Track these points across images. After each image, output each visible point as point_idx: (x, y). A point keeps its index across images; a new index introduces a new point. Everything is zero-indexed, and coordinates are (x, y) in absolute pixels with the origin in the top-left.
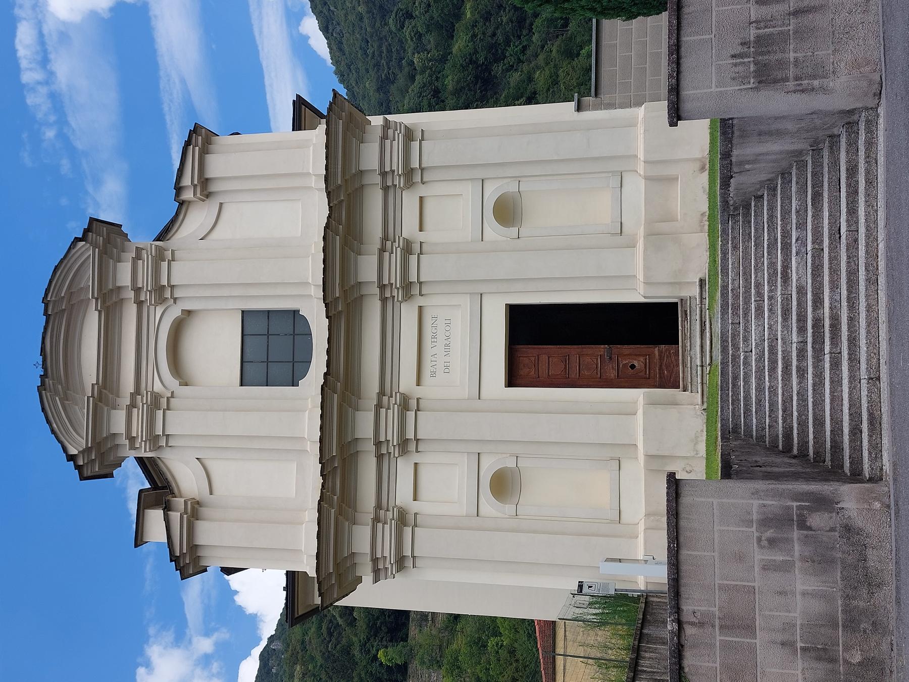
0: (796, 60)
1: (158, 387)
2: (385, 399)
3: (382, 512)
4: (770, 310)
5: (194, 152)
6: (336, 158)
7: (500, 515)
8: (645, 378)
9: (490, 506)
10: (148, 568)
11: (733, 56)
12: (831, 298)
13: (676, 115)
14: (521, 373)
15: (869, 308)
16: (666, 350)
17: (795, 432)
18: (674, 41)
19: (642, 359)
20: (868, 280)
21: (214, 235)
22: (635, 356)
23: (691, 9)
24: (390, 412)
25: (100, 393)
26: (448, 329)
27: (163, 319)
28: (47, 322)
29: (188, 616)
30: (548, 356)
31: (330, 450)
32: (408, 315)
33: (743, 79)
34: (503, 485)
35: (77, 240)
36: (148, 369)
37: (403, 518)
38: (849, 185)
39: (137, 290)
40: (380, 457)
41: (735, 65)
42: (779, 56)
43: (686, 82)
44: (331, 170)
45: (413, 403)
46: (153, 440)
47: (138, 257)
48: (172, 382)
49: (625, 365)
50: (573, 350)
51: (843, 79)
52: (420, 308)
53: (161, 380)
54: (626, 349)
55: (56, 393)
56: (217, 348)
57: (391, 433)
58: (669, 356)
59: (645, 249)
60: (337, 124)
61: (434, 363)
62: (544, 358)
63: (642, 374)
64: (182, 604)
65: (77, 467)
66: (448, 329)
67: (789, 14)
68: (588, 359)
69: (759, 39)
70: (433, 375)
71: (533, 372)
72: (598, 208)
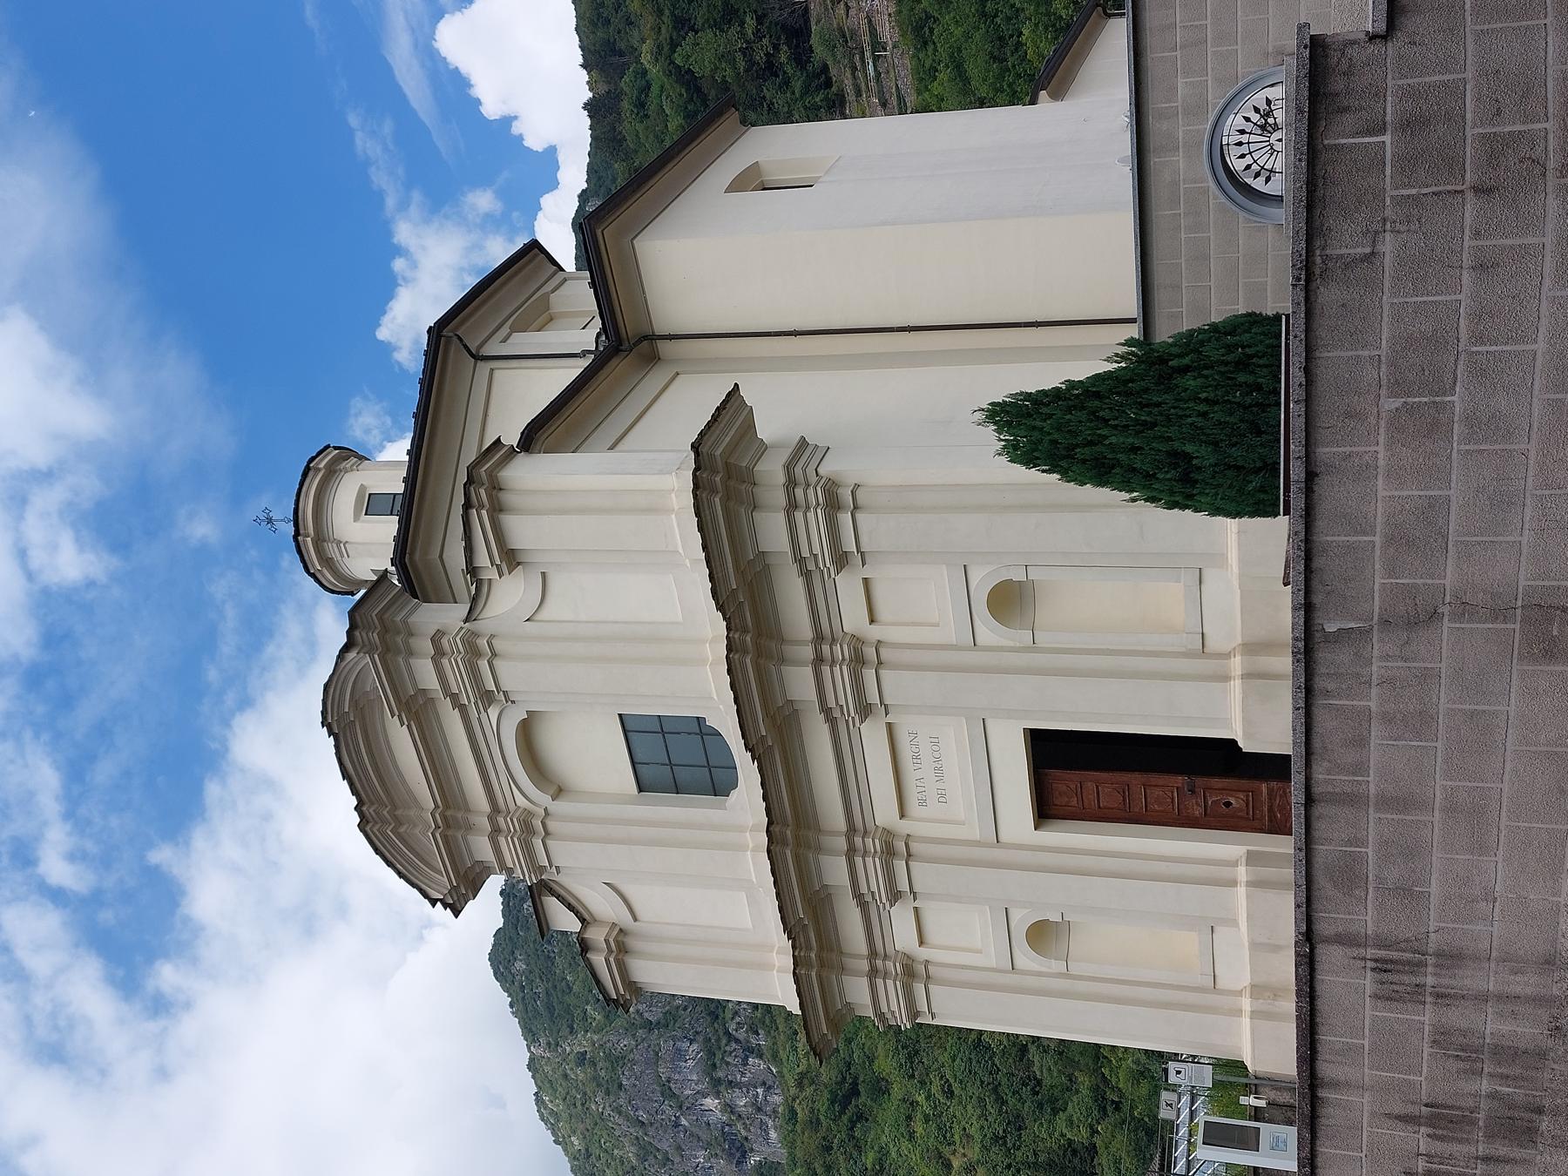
2: (799, 492)
7: (1044, 969)
9: (990, 631)
18: (1304, 928)
21: (543, 615)
23: (1332, 1121)
24: (811, 515)
25: (444, 818)
27: (504, 725)
28: (336, 740)
30: (1102, 785)
31: (757, 729)
32: (872, 736)
35: (346, 649)
36: (501, 783)
37: (910, 971)
40: (807, 575)
45: (870, 652)
47: (439, 653)
48: (543, 799)
50: (1135, 779)
53: (525, 794)
54: (1217, 782)
55: (384, 822)
56: (594, 756)
57: (873, 881)
60: (711, 506)
62: (1090, 786)
64: (389, 69)
65: (446, 906)
68: (1157, 792)
70: (923, 802)
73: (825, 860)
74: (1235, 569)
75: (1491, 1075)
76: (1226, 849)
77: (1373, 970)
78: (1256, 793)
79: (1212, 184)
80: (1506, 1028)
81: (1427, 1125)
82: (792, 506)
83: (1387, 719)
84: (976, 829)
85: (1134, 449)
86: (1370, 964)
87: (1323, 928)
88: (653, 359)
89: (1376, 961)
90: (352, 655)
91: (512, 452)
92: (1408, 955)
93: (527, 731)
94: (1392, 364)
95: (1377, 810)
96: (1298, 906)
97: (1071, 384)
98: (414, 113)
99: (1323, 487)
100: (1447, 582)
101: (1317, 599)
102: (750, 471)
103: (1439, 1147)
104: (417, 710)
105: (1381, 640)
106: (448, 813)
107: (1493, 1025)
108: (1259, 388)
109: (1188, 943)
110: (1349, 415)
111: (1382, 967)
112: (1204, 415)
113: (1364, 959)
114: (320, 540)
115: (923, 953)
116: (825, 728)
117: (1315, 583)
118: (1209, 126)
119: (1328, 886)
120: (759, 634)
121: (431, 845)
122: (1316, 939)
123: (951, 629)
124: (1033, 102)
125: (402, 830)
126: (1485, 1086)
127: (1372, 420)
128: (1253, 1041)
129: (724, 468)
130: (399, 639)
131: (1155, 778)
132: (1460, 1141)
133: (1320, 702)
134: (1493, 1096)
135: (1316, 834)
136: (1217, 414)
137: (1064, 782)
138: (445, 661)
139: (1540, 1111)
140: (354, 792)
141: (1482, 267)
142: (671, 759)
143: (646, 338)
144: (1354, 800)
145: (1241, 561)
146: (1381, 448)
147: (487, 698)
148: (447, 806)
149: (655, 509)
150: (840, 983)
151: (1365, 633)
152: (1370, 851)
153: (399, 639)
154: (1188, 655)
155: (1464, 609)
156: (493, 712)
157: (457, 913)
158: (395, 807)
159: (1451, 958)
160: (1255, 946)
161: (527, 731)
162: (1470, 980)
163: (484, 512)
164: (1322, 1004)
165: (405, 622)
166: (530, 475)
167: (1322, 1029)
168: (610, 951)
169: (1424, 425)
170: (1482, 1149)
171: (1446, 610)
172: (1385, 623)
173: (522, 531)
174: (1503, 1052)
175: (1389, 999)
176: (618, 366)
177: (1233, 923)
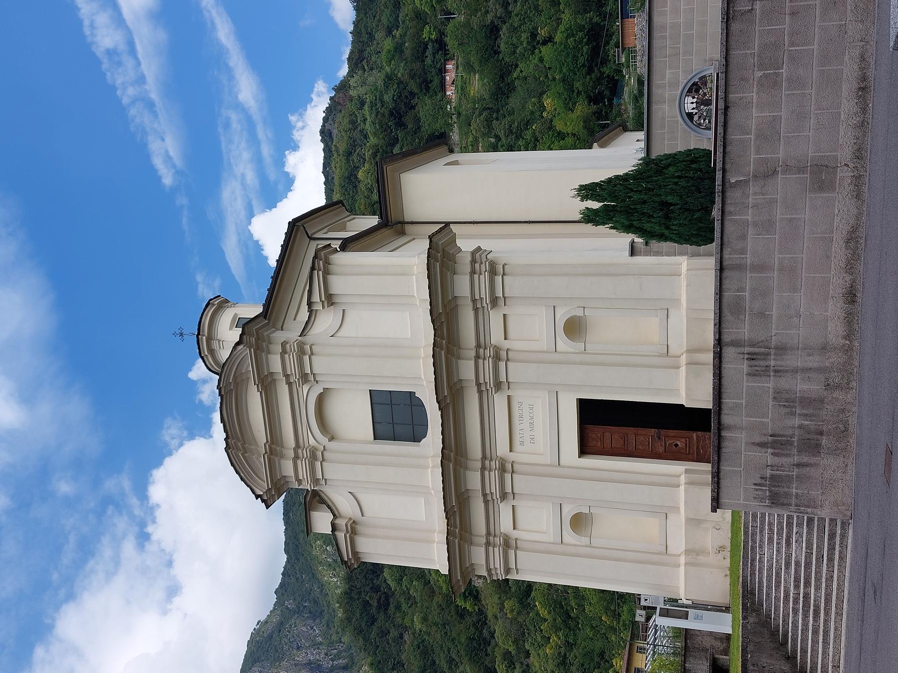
0: (797, 495)
1: (312, 442)
2: (477, 265)
3: (491, 538)
4: (777, 551)
5: (318, 276)
6: (437, 293)
7: (578, 543)
10: (185, 221)
11: (755, 484)
12: (815, 595)
13: (716, 504)
15: (836, 629)
17: (790, 634)
20: (837, 613)
21: (340, 334)
24: (482, 277)
27: (309, 394)
29: (230, 264)
30: (612, 434)
33: (762, 500)
34: (579, 522)
35: (238, 344)
37: (507, 544)
38: (829, 544)
39: (287, 376)
41: (757, 490)
42: (786, 490)
43: (722, 495)
44: (434, 304)
45: (503, 354)
46: (316, 481)
47: (284, 352)
48: (324, 440)
50: (630, 430)
51: (827, 511)
52: (509, 396)
53: (314, 438)
54: (672, 433)
55: (238, 449)
56: (354, 416)
58: (704, 440)
60: (435, 268)
62: (608, 435)
64: (222, 253)
65: (263, 501)
67: (794, 465)
68: (641, 438)
69: (772, 477)
70: (522, 443)
72: (650, 327)
73: (469, 473)
74: (685, 306)
75: (799, 415)
76: (676, 469)
77: (747, 359)
78: (691, 438)
79: (680, 119)
80: (805, 387)
81: (772, 448)
82: (473, 272)
83: (755, 224)
84: (548, 458)
85: (644, 202)
86: (746, 356)
87: (726, 338)
88: (402, 233)
89: (748, 354)
90: (241, 347)
91: (336, 251)
92: (762, 350)
93: (321, 400)
94: (759, 56)
95: (750, 272)
96: (715, 325)
97: (617, 177)
98: (233, 276)
99: (732, 112)
100: (780, 156)
101: (728, 167)
102: (454, 256)
103: (777, 460)
104: (267, 384)
105: (753, 185)
106: (273, 446)
107: (801, 386)
108: (701, 170)
109: (651, 526)
110: (742, 79)
111: (752, 357)
112: (676, 184)
113: (743, 353)
114: (210, 339)
115: (515, 534)
116: (477, 395)
117: (727, 160)
118: (679, 92)
119: (729, 314)
120: (448, 343)
121: (261, 463)
122: (723, 344)
123: (544, 343)
124: (590, 148)
125: (246, 455)
126: (797, 421)
127: (751, 81)
128: (686, 580)
129: (441, 256)
130: (264, 344)
131: (641, 431)
132: (787, 455)
133: (728, 217)
134: (801, 427)
135: (724, 287)
136: (683, 183)
137: (596, 431)
138: (287, 356)
139: (821, 433)
140: (225, 431)
141: (793, 14)
142: (396, 418)
143: (400, 223)
144: (740, 267)
145: (688, 301)
146: (754, 94)
147: (304, 378)
148: (272, 443)
149: (404, 273)
150: (469, 551)
151: (746, 182)
152: (747, 294)
153: (264, 344)
154: (661, 356)
155: (787, 169)
156: (306, 388)
157: (268, 507)
158: (244, 443)
159: (782, 349)
160: (689, 520)
161: (321, 400)
162: (793, 361)
163: (321, 272)
164: (724, 381)
165: (268, 336)
166: (343, 259)
167: (724, 396)
168: (347, 531)
169: (771, 83)
170: (796, 459)
171: (779, 169)
172: (755, 176)
173: (338, 284)
174: (806, 401)
175: (754, 375)
176: (386, 232)
177: (678, 509)
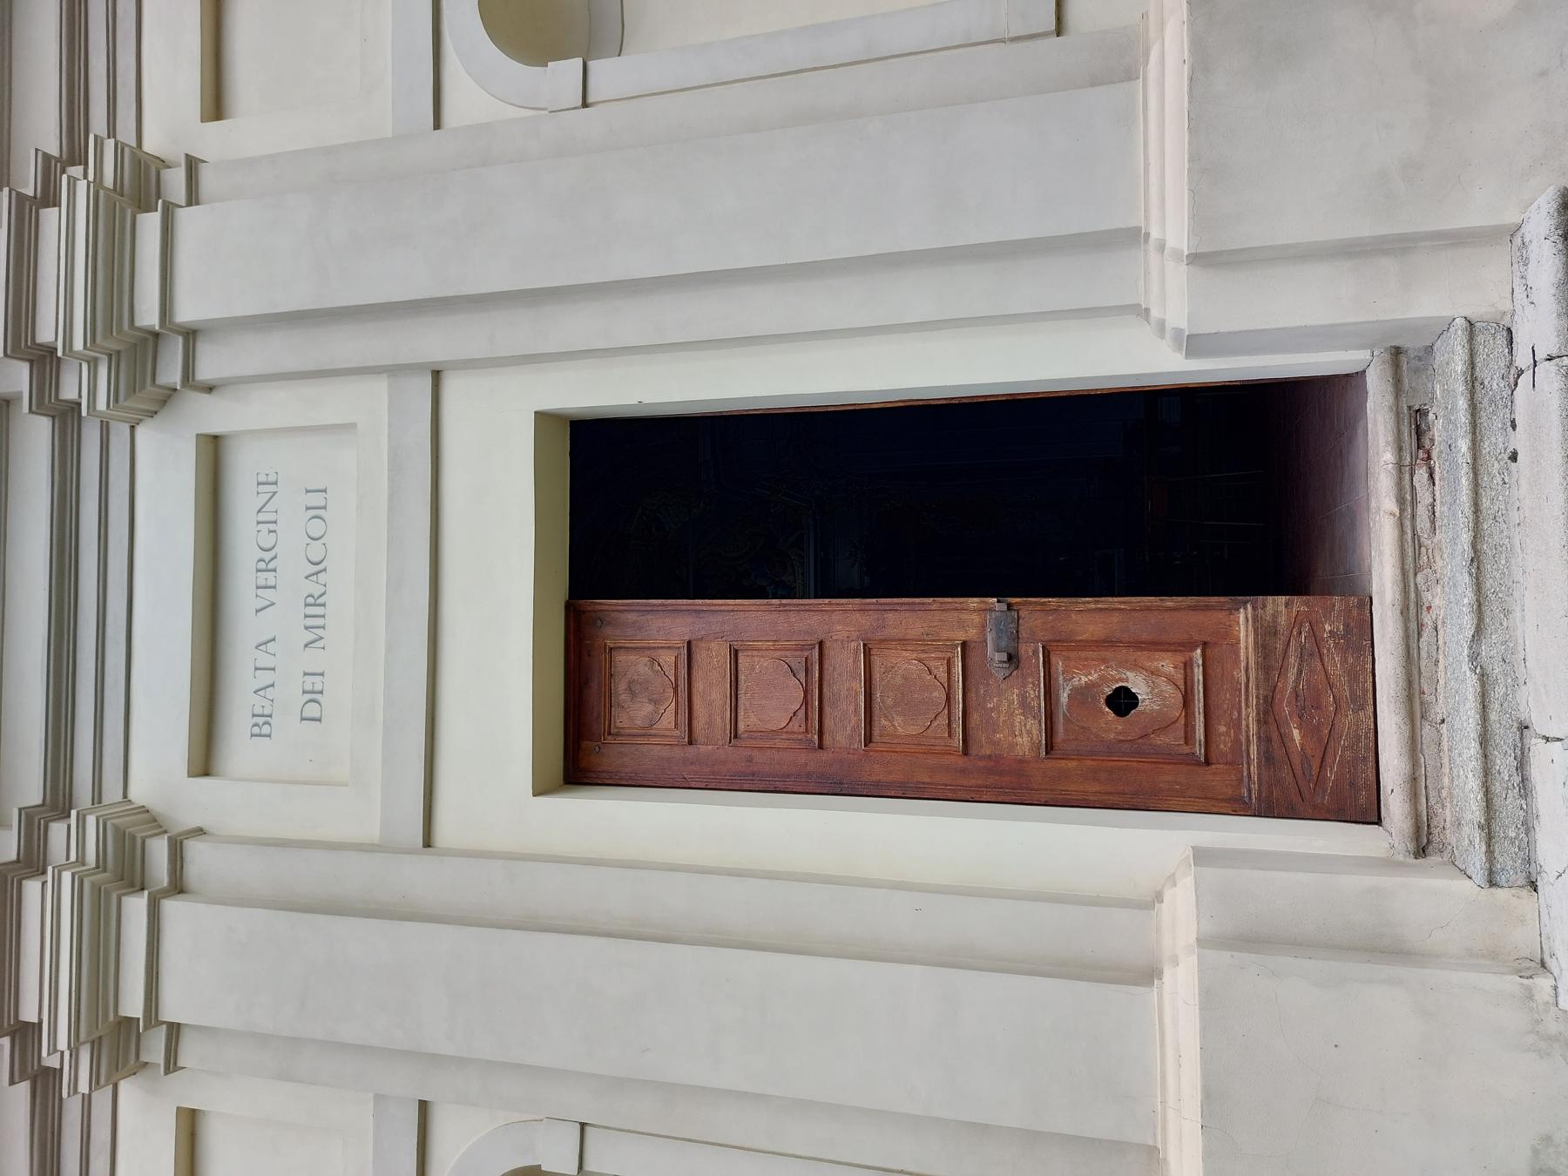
8: (1189, 760)
14: (622, 720)
16: (1297, 622)
19: (1167, 664)
22: (1134, 651)
26: (316, 528)
32: (162, 468)
49: (1080, 695)
54: (1089, 616)
59: (1201, 65)
61: (265, 678)
63: (1171, 740)
66: (316, 528)
70: (262, 724)
71: (668, 720)
